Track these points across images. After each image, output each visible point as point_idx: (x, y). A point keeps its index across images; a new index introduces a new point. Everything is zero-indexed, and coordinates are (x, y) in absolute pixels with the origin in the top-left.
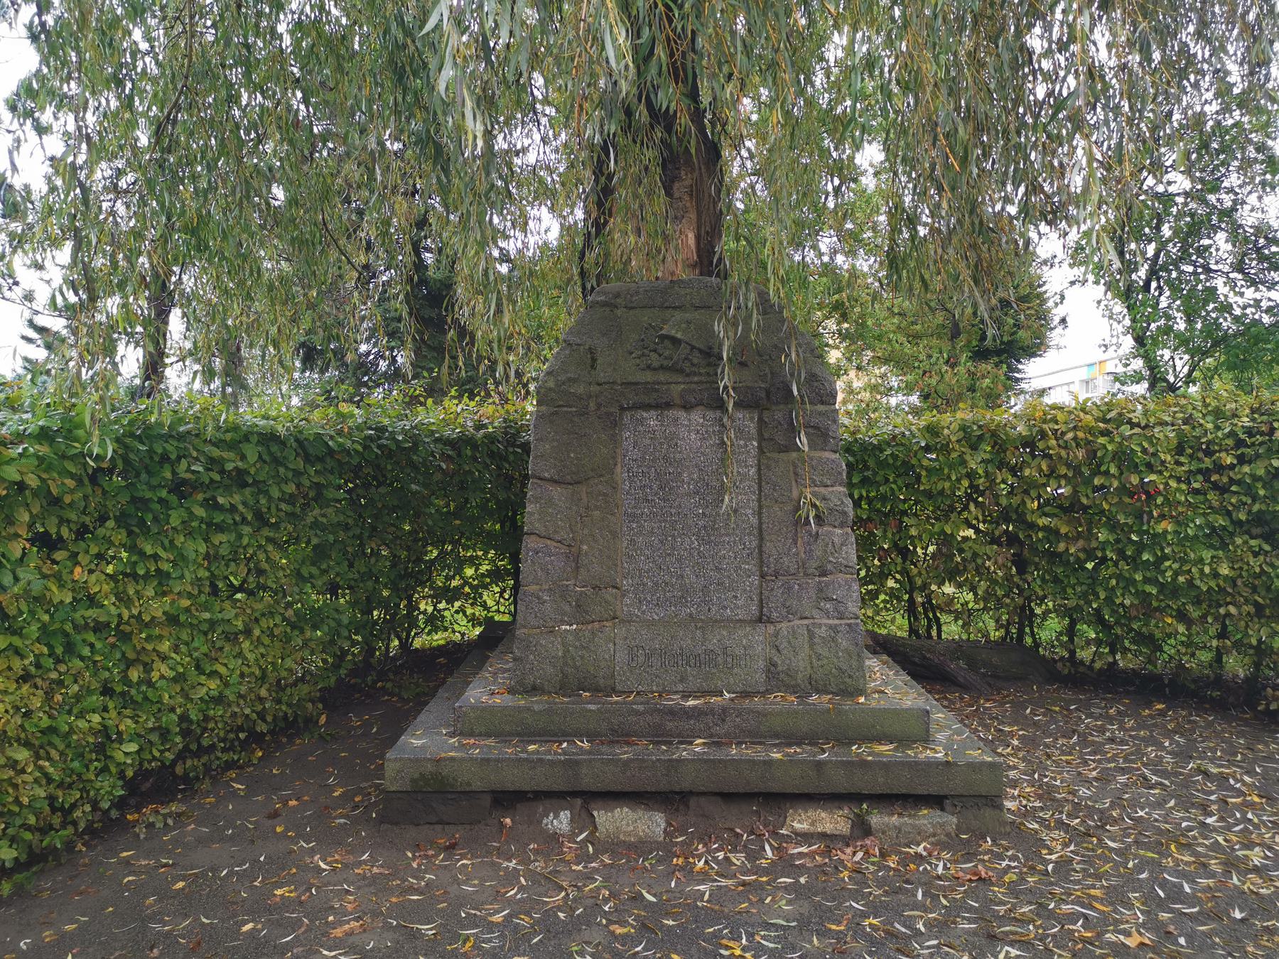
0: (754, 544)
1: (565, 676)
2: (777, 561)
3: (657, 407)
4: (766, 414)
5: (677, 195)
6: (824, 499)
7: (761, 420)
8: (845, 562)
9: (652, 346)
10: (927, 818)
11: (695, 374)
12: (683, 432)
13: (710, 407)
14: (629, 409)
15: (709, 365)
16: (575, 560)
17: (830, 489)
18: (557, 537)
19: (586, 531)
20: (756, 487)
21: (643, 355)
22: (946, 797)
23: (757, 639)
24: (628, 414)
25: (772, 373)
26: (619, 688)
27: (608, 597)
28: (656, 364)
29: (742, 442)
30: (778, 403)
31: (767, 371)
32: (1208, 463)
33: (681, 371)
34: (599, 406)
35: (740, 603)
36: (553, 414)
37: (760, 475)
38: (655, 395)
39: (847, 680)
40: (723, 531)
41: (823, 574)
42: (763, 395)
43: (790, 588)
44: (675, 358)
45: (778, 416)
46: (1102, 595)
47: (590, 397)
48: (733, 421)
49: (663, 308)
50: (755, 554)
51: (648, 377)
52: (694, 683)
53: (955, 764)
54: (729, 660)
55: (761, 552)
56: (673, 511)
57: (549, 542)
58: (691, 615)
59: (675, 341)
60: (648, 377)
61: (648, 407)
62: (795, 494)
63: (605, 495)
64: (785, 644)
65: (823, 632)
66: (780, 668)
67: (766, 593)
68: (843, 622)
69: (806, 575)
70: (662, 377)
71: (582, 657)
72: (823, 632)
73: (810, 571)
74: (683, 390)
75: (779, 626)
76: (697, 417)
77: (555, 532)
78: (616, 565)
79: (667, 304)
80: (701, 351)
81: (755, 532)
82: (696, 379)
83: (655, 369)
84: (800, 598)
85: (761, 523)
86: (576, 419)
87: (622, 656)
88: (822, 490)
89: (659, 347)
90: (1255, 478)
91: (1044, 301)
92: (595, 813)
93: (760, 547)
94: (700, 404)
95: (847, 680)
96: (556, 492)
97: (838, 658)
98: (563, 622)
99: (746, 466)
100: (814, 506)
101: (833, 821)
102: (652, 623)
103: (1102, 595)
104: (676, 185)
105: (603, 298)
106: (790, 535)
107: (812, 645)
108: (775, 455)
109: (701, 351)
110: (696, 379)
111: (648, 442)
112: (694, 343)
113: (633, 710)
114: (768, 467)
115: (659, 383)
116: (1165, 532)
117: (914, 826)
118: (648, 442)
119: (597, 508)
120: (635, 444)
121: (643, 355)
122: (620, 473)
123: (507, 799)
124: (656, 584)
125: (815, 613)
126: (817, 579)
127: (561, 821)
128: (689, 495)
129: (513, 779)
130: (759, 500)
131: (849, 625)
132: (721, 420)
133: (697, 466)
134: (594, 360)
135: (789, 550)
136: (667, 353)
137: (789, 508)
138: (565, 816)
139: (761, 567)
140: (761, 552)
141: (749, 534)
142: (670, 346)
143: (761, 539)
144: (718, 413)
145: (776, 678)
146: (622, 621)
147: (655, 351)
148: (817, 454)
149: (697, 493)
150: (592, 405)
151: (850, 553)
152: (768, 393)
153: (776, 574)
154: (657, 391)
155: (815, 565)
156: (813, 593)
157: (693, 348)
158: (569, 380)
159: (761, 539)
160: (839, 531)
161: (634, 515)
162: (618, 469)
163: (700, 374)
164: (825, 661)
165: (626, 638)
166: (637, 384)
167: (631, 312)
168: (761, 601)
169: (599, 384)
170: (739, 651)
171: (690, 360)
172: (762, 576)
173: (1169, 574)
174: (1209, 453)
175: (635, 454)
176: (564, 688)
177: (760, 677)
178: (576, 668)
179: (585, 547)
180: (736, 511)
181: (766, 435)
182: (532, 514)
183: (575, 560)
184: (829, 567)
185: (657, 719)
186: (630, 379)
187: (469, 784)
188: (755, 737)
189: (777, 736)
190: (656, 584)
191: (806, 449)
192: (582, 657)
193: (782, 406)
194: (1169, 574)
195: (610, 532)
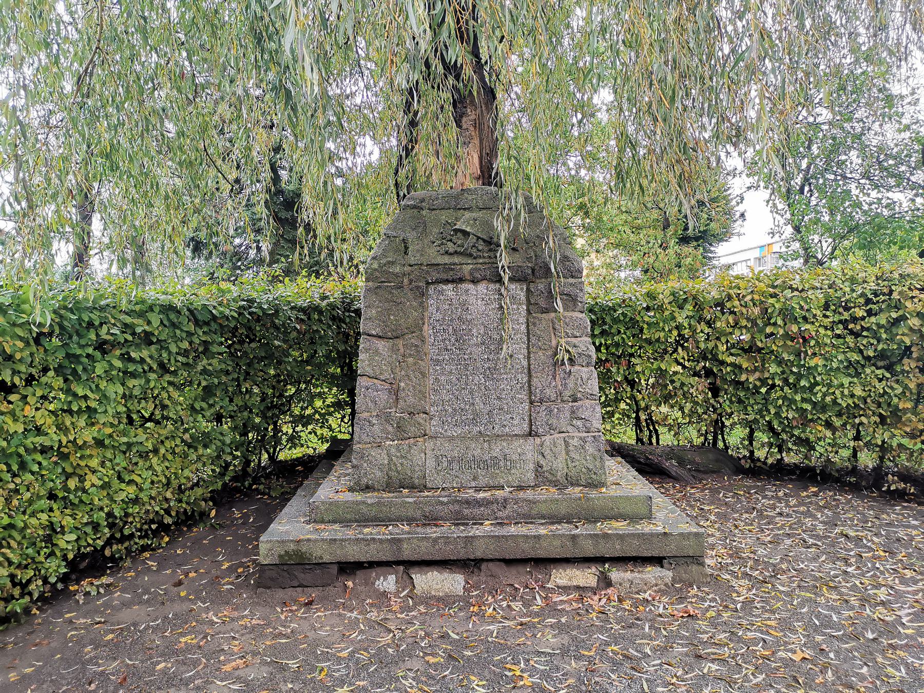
0: (525, 379)
1: (390, 478)
2: (541, 391)
3: (453, 281)
5: (464, 126)
7: (528, 290)
8: (590, 392)
9: (449, 237)
10: (652, 573)
12: (472, 300)
13: (491, 281)
14: (432, 283)
15: (490, 250)
16: (396, 393)
17: (579, 339)
18: (382, 377)
19: (403, 373)
21: (442, 244)
22: (664, 558)
23: (528, 447)
24: (432, 287)
26: (429, 485)
28: (451, 250)
29: (515, 306)
32: (846, 316)
33: (471, 255)
34: (411, 281)
35: (515, 422)
37: (528, 330)
38: (451, 273)
39: (593, 476)
40: (502, 371)
41: (575, 400)
42: (530, 272)
43: (551, 411)
45: (541, 286)
46: (773, 411)
47: (404, 275)
48: (509, 291)
49: (457, 209)
51: (446, 260)
52: (482, 481)
53: (671, 534)
54: (508, 463)
55: (530, 386)
56: (466, 357)
58: (480, 432)
59: (466, 234)
60: (446, 260)
61: (447, 282)
62: (554, 343)
64: (548, 451)
65: (575, 442)
66: (545, 469)
67: (534, 415)
69: (563, 401)
70: (456, 259)
71: (402, 464)
72: (575, 442)
73: (565, 399)
76: (482, 287)
80: (484, 240)
82: (481, 261)
83: (451, 254)
84: (558, 418)
85: (529, 365)
86: (394, 291)
87: (431, 463)
88: (573, 340)
89: (454, 238)
90: (879, 326)
92: (413, 576)
93: (529, 382)
94: (484, 279)
95: (593, 476)
96: (381, 345)
98: (387, 438)
100: (568, 351)
101: (586, 577)
102: (451, 439)
103: (773, 411)
104: (464, 119)
105: (412, 202)
106: (550, 373)
107: (567, 453)
108: (539, 315)
109: (484, 240)
110: (481, 261)
111: (447, 307)
112: (479, 235)
113: (440, 501)
114: (534, 324)
115: (454, 264)
116: (817, 365)
117: (642, 579)
118: (447, 307)
119: (410, 355)
121: (442, 244)
122: (427, 330)
123: (348, 568)
124: (455, 410)
125: (570, 428)
126: (570, 404)
127: (388, 582)
128: (477, 345)
129: (353, 553)
130: (528, 348)
131: (594, 437)
134: (406, 248)
135: (550, 383)
136: (459, 242)
137: (550, 353)
138: (392, 578)
140: (530, 386)
141: (521, 373)
142: (462, 237)
143: (530, 376)
144: (498, 286)
145: (542, 476)
147: (451, 240)
148: (566, 314)
149: (483, 344)
150: (406, 281)
151: (594, 385)
152: (533, 270)
154: (452, 270)
155: (569, 394)
156: (568, 414)
157: (478, 238)
159: (530, 376)
161: (438, 360)
162: (426, 327)
163: (484, 257)
166: (438, 265)
168: (531, 420)
169: (410, 266)
170: (515, 457)
172: (531, 403)
173: (819, 395)
174: (847, 309)
175: (439, 316)
176: (389, 486)
177: (531, 475)
178: (398, 472)
179: (402, 384)
180: (511, 356)
181: (533, 301)
182: (363, 363)
183: (396, 393)
184: (579, 395)
185: (457, 507)
186: (433, 262)
187: (321, 558)
188: (528, 519)
189: (543, 517)
190: (455, 410)
191: (561, 310)
194: (819, 395)
195: (421, 373)
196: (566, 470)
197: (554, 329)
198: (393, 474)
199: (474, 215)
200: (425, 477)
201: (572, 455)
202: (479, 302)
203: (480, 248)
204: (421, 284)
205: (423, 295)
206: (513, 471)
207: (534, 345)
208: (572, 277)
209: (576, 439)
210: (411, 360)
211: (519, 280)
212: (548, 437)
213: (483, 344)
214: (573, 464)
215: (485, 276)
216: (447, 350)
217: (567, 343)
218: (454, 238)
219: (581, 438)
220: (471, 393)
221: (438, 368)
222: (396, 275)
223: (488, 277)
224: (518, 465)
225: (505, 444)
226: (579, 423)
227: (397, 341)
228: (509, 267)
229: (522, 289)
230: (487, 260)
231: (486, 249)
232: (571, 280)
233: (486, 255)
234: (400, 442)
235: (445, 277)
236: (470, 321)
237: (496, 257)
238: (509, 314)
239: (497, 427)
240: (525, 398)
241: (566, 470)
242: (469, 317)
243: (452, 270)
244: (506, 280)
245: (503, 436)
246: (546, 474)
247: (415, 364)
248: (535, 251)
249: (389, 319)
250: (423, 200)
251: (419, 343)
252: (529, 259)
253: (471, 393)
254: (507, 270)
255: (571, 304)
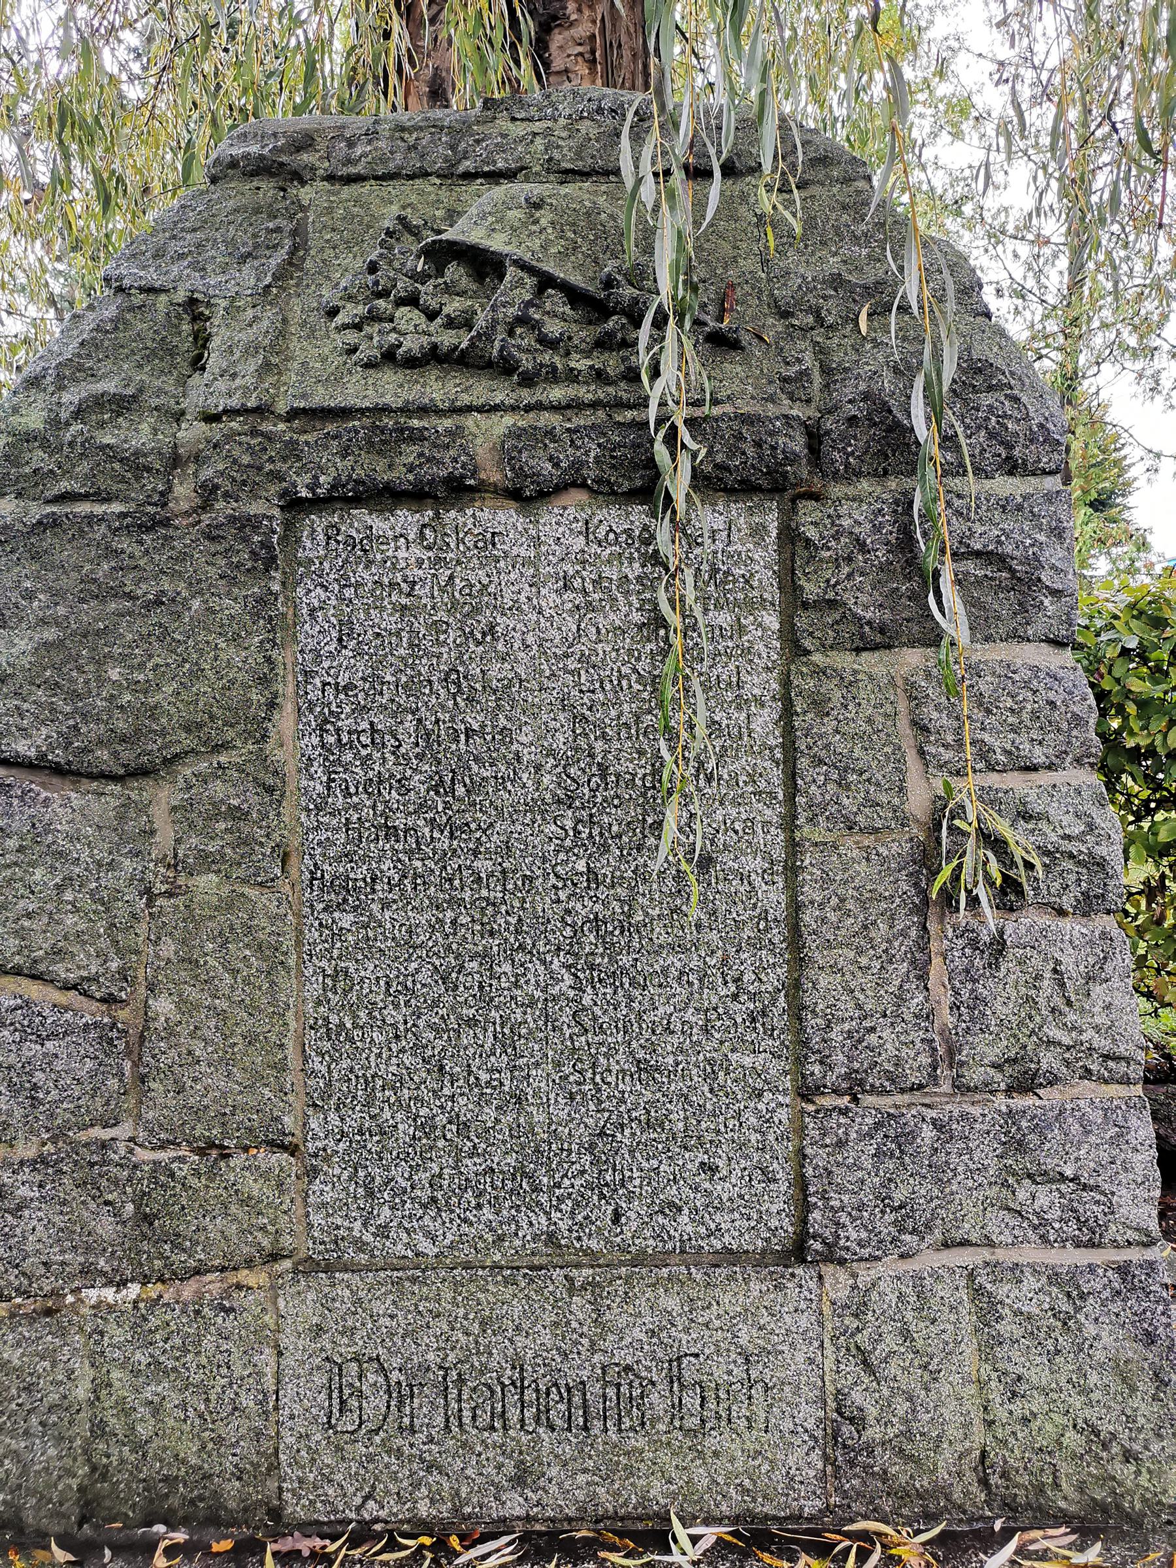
0: (775, 977)
1: (100, 1472)
2: (855, 1039)
3: (416, 496)
4: (809, 518)
5: (558, 64)
6: (1025, 815)
7: (790, 536)
8: (1102, 1043)
9: (403, 285)
11: (553, 376)
14: (318, 504)
15: (603, 344)
17: (1044, 778)
19: (168, 948)
20: (776, 775)
24: (318, 522)
25: (826, 371)
26: (296, 1510)
27: (253, 1186)
28: (412, 344)
29: (724, 618)
30: (852, 474)
31: (809, 360)
33: (505, 367)
36: (40, 525)
37: (789, 732)
38: (410, 454)
39: (1123, 1471)
41: (1026, 1084)
42: (798, 444)
43: (905, 1138)
44: (481, 320)
47: (175, 461)
48: (692, 542)
49: (451, 176)
50: (778, 1016)
54: (691, 1401)
55: (797, 1011)
56: (483, 865)
57: (33, 990)
58: (551, 1238)
62: (918, 801)
63: (239, 815)
64: (891, 1342)
66: (874, 1433)
67: (819, 1156)
68: (1097, 1257)
69: (961, 1088)
71: (156, 1409)
73: (975, 1075)
74: (516, 433)
75: (866, 1275)
77: (57, 953)
78: (281, 1067)
79: (467, 165)
80: (574, 296)
81: (776, 935)
82: (557, 394)
83: (412, 363)
84: (940, 1174)
85: (796, 907)
86: (124, 543)
88: (1015, 782)
89: (426, 290)
91: (1123, 471)
93: (794, 988)
94: (572, 482)
95: (1123, 1471)
97: (1085, 1391)
98: (87, 1271)
99: (741, 703)
100: (997, 845)
104: (557, 39)
106: (901, 947)
107: (989, 1347)
108: (844, 661)
109: (574, 296)
110: (557, 394)
111: (390, 621)
112: (549, 267)
114: (819, 705)
115: (424, 411)
118: (390, 621)
119: (207, 862)
120: (345, 632)
121: (374, 317)
124: (427, 1127)
125: (997, 1224)
126: (1001, 1102)
128: (535, 807)
130: (789, 823)
131: (1123, 1270)
132: (648, 538)
133: (564, 703)
134: (202, 340)
135: (900, 999)
136: (453, 306)
137: (897, 846)
139: (801, 1061)
140: (797, 1011)
141: (755, 945)
142: (465, 282)
143: (798, 959)
144: (638, 515)
146: (308, 1267)
147: (412, 300)
149: (567, 801)
150: (184, 492)
152: (814, 437)
153: (855, 1087)
154: (417, 437)
155: (993, 1053)
156: (987, 1153)
157: (546, 282)
158: (98, 402)
159: (798, 959)
160: (1072, 927)
161: (345, 885)
162: (285, 721)
163: (572, 377)
164: (1037, 1403)
165: (319, 1330)
166: (344, 413)
167: (347, 192)
168: (801, 1183)
169: (211, 418)
171: (534, 326)
172: (806, 1092)
178: (140, 1446)
179: (163, 1006)
180: (706, 863)
181: (811, 590)
184: (1049, 1060)
186: (321, 397)
190: (427, 1127)
191: (962, 634)
192: (156, 1409)
193: (865, 485)
196: (979, 1436)
197: (921, 727)
198: (117, 1454)
199: (535, 190)
200: (274, 1467)
201: (1016, 1359)
202: (549, 598)
203: (553, 328)
204: (255, 508)
205: (271, 562)
206: (711, 1442)
207: (816, 812)
208: (1012, 467)
209: (1031, 1282)
210: (206, 883)
211: (744, 489)
212: (889, 1267)
213: (567, 801)
214: (1017, 1407)
215: (578, 465)
216: (391, 832)
217: (990, 799)
218: (426, 290)
219: (1054, 1278)
220: (507, 1042)
221: (346, 920)
222: (136, 464)
223: (591, 474)
224: (740, 1410)
225: (671, 1303)
226: (1045, 1198)
227: (137, 791)
228: (690, 422)
229: (758, 532)
230: (585, 393)
231: (583, 335)
232: (1005, 486)
233: (580, 363)
234: (153, 1290)
235: (383, 471)
236: (502, 692)
237: (632, 376)
238: (693, 654)
239: (634, 1212)
240: (775, 1067)
241: (979, 1436)
242: (497, 671)
243: (417, 437)
244: (679, 484)
245: (661, 1260)
246: (883, 1458)
247: (229, 905)
248: (821, 351)
249: (101, 681)
250: (305, 142)
251: (253, 799)
252: (794, 385)
253: (507, 1042)
254: (684, 434)
255: (1003, 605)
